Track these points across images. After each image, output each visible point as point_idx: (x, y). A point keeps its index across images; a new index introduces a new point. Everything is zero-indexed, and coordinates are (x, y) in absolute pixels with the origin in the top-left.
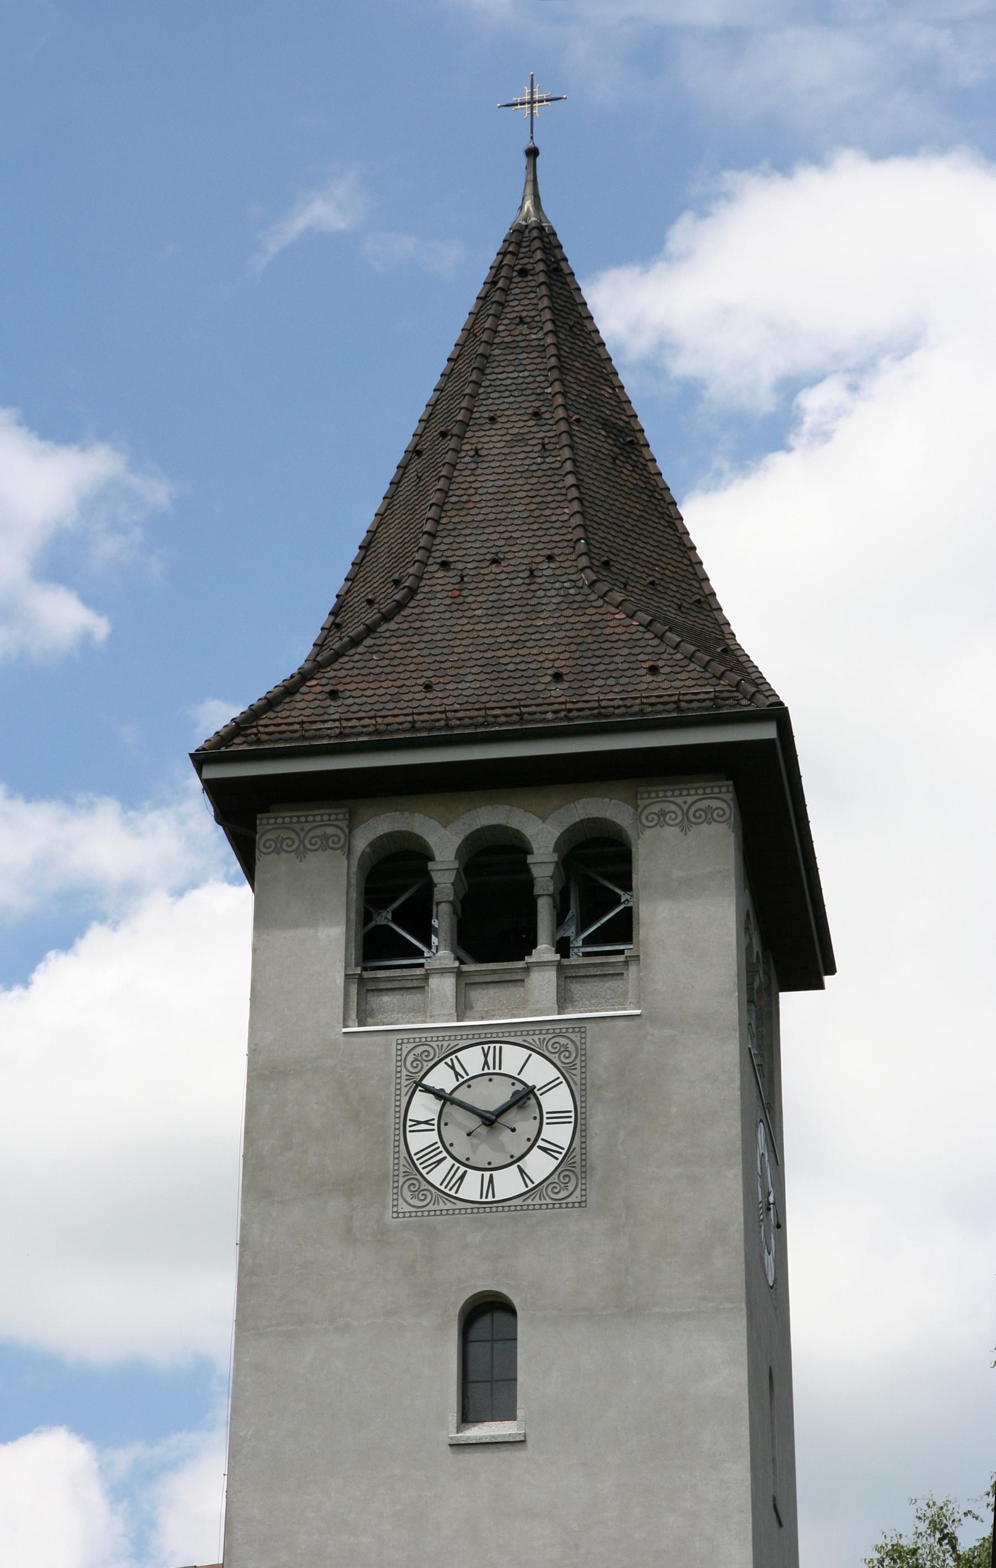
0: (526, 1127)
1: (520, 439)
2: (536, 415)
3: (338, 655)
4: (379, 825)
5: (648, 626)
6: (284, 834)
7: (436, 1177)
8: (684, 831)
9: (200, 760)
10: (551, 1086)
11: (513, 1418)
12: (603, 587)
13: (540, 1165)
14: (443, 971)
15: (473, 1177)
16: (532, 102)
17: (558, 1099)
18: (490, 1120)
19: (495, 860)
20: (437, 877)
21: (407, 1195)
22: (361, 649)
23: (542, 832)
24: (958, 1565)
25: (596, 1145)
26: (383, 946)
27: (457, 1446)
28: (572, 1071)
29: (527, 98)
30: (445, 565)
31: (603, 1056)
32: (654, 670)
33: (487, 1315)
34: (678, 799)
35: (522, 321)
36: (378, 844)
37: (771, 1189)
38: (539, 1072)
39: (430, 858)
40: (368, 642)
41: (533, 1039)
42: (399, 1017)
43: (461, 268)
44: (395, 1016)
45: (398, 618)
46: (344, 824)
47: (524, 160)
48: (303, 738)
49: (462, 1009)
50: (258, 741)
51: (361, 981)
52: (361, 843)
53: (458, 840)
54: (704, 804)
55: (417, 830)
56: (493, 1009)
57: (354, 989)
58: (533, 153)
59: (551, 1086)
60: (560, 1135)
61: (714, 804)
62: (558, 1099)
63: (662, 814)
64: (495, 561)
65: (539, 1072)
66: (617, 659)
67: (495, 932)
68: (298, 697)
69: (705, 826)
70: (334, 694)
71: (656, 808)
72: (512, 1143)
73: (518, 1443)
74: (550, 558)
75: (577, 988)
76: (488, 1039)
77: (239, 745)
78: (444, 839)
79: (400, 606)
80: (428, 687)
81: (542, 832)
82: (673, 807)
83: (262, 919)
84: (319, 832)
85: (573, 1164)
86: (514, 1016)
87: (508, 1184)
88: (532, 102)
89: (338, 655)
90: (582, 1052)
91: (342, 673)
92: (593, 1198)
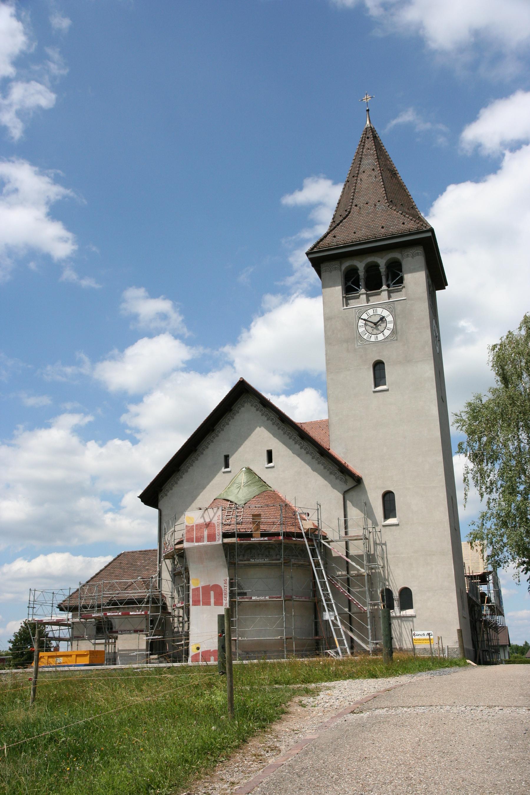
0: (383, 325)
2: (373, 170)
4: (347, 264)
5: (401, 214)
7: (365, 337)
10: (388, 316)
13: (387, 333)
17: (390, 318)
18: (375, 324)
23: (382, 262)
25: (399, 327)
26: (350, 290)
27: (374, 392)
28: (392, 312)
30: (356, 206)
31: (399, 307)
32: (403, 223)
33: (379, 368)
36: (346, 268)
40: (341, 224)
42: (353, 303)
51: (346, 297)
52: (343, 268)
53: (364, 265)
54: (417, 252)
56: (374, 300)
57: (344, 299)
59: (388, 316)
60: (391, 326)
61: (419, 251)
62: (390, 318)
63: (408, 255)
64: (367, 203)
67: (373, 285)
70: (335, 237)
73: (273, 467)
74: (379, 201)
76: (374, 307)
77: (315, 250)
78: (361, 265)
80: (355, 233)
81: (382, 262)
85: (394, 332)
87: (381, 337)
88: (53, 631)
90: (394, 308)
92: (399, 338)
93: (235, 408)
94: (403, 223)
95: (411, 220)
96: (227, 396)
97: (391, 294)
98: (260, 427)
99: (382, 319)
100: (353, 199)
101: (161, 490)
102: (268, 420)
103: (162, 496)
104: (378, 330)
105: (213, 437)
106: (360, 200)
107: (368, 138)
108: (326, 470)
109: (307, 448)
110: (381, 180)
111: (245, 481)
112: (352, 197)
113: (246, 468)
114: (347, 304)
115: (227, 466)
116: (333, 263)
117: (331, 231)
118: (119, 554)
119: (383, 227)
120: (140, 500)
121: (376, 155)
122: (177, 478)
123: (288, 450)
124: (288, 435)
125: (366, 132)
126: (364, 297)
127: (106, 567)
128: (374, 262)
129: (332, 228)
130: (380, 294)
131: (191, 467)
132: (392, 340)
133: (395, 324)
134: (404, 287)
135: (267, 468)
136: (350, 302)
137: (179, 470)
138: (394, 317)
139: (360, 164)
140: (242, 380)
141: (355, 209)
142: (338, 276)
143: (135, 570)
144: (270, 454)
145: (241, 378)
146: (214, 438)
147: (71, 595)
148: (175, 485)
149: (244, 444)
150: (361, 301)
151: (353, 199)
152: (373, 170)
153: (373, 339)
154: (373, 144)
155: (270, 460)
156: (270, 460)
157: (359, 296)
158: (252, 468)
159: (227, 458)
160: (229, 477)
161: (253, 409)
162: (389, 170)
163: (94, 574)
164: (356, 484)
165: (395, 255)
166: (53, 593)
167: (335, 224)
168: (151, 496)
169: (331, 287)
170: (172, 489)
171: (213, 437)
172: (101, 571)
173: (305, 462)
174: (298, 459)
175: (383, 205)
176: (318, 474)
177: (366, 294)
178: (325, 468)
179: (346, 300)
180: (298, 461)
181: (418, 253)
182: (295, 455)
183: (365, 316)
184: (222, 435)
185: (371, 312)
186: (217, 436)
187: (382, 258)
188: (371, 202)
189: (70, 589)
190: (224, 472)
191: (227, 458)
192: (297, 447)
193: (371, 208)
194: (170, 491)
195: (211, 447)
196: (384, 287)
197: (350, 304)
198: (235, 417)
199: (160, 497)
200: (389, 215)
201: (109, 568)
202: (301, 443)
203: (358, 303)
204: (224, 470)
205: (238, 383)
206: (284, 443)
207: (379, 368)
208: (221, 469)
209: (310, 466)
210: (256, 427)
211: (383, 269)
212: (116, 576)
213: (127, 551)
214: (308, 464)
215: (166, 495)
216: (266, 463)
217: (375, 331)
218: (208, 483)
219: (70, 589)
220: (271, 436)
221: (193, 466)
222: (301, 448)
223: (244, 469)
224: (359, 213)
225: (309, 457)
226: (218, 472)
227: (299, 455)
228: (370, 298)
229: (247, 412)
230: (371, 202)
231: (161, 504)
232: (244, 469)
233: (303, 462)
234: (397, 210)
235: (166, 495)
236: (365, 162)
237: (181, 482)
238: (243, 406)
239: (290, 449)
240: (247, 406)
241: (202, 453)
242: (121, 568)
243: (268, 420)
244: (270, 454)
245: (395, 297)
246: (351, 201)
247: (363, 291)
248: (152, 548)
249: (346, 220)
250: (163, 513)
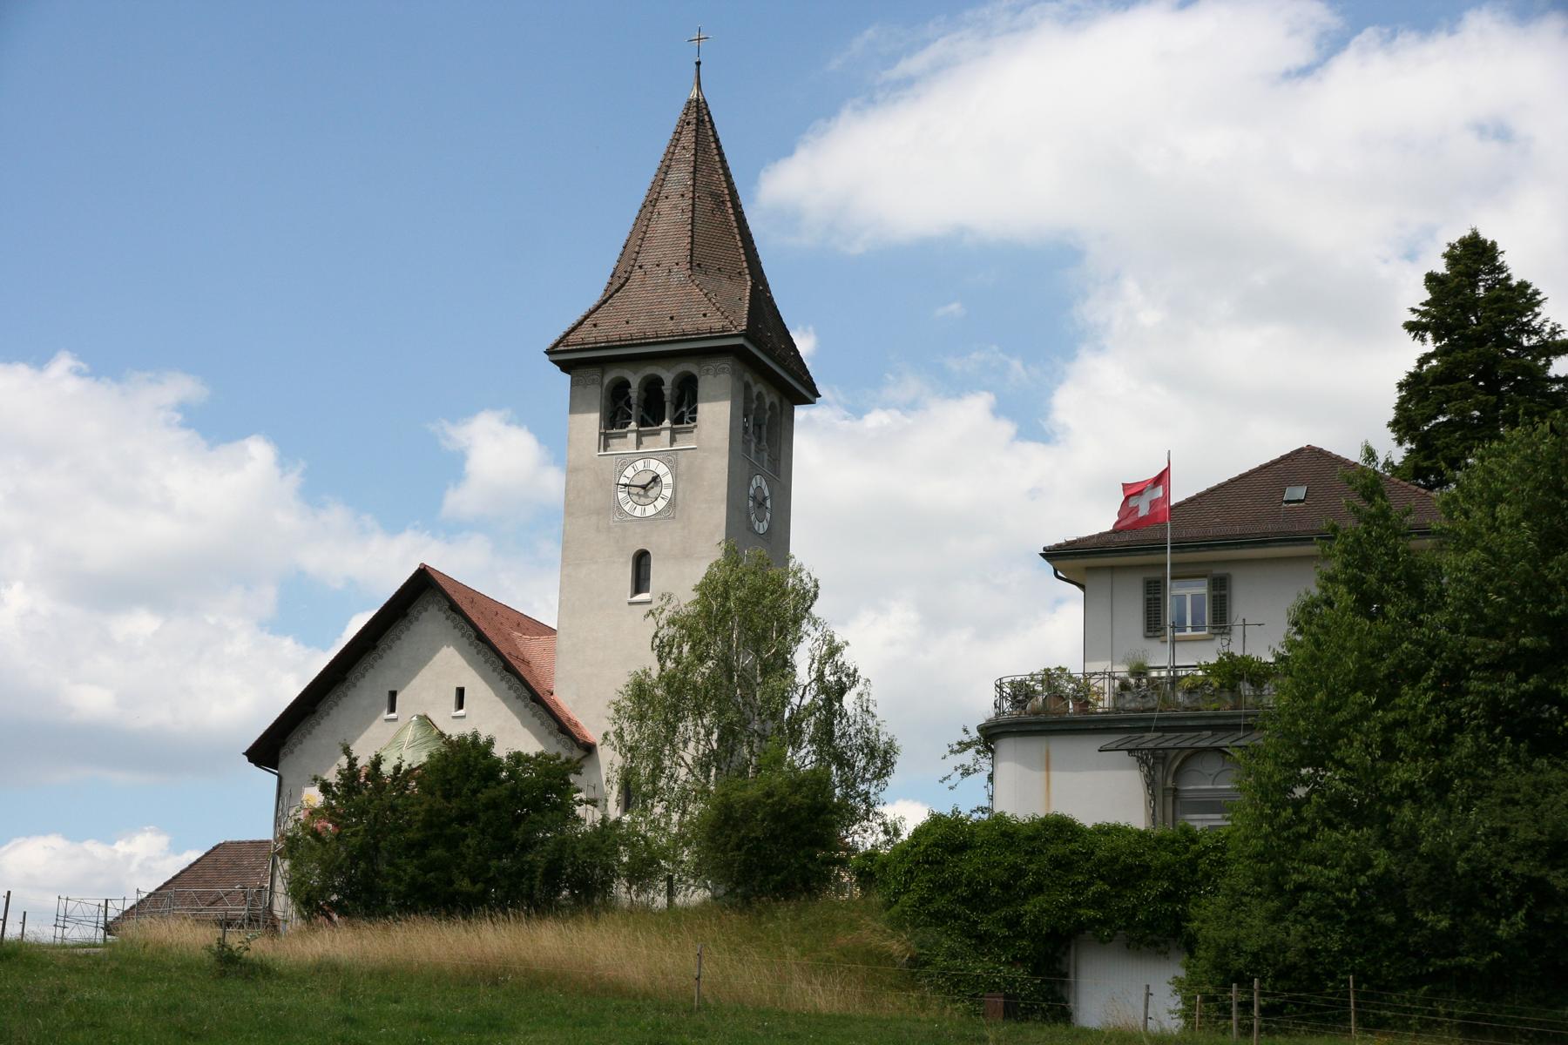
0: (656, 490)
1: (675, 207)
4: (612, 374)
7: (626, 508)
9: (548, 352)
13: (661, 504)
17: (667, 479)
18: (644, 487)
19: (652, 387)
23: (668, 376)
25: (679, 496)
26: (614, 420)
28: (674, 469)
31: (683, 461)
33: (641, 561)
36: (611, 381)
38: (662, 469)
43: (673, 115)
49: (639, 443)
52: (606, 381)
56: (650, 444)
58: (698, 63)
60: (667, 492)
62: (667, 479)
67: (651, 415)
73: (463, 717)
76: (646, 456)
77: (561, 348)
78: (635, 379)
81: (668, 376)
83: (573, 384)
85: (672, 503)
87: (650, 510)
93: (413, 612)
99: (656, 479)
101: (284, 744)
106: (647, 259)
114: (606, 446)
115: (392, 710)
116: (591, 370)
117: (605, 302)
126: (632, 437)
133: (675, 491)
136: (613, 442)
137: (314, 712)
138: (675, 478)
141: (638, 273)
142: (596, 394)
144: (461, 692)
155: (460, 705)
156: (460, 705)
160: (393, 727)
161: (442, 616)
162: (712, 194)
175: (681, 273)
179: (606, 439)
183: (623, 481)
185: (640, 465)
186: (381, 657)
188: (665, 263)
192: (504, 685)
193: (661, 273)
195: (370, 675)
196: (667, 423)
200: (687, 294)
204: (386, 715)
207: (641, 561)
214: (518, 714)
224: (643, 283)
225: (520, 704)
226: (375, 718)
227: (505, 700)
229: (429, 621)
230: (665, 263)
236: (673, 176)
237: (317, 731)
244: (461, 692)
245: (684, 442)
248: (265, 838)
250: (285, 782)
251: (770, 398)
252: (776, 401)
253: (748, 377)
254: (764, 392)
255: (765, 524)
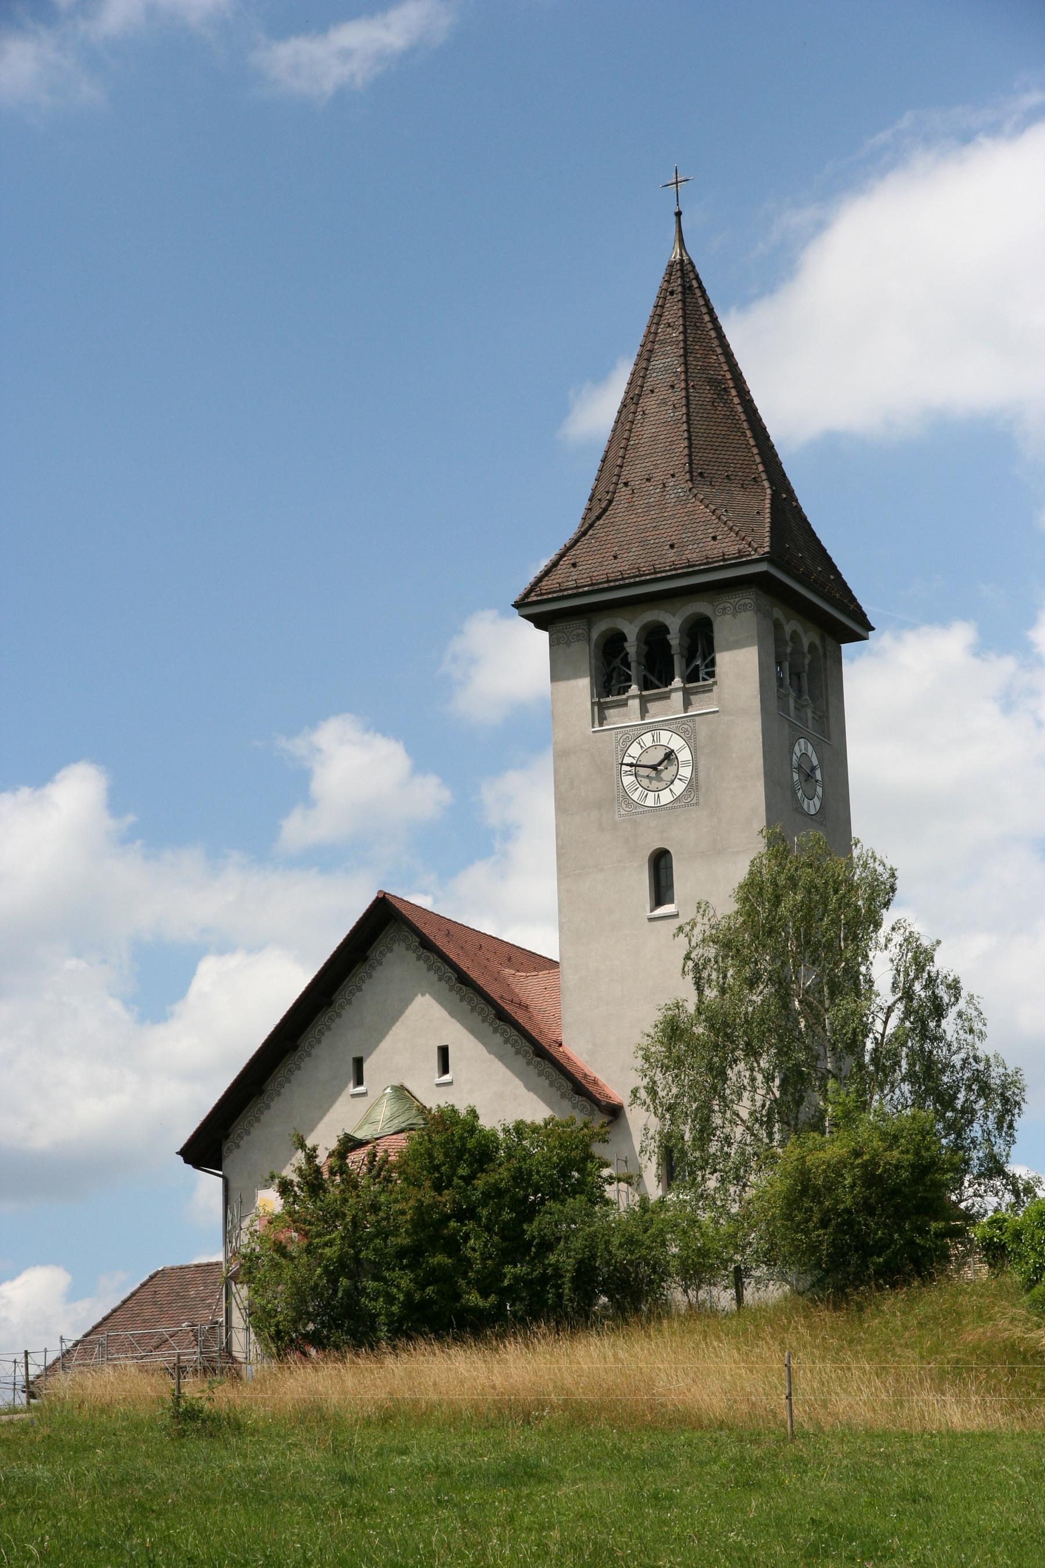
0: (672, 769)
1: (664, 402)
2: (672, 387)
3: (591, 526)
4: (602, 626)
5: (713, 512)
6: (560, 635)
7: (635, 797)
8: (734, 616)
10: (681, 749)
11: (672, 902)
12: (695, 491)
13: (679, 787)
14: (633, 697)
15: (651, 795)
16: (677, 183)
17: (684, 755)
18: (654, 767)
20: (628, 650)
21: (624, 806)
22: (587, 537)
23: (674, 621)
24: (3, 1426)
25: (702, 775)
26: (609, 684)
27: (651, 919)
29: (674, 181)
30: (626, 484)
31: (703, 729)
32: (714, 538)
33: (660, 864)
34: (730, 601)
35: (669, 326)
37: (815, 762)
38: (676, 743)
39: (626, 640)
40: (591, 532)
41: (673, 727)
42: (617, 718)
44: (615, 719)
45: (604, 517)
46: (586, 627)
47: (674, 218)
48: (561, 591)
49: (644, 712)
50: (542, 594)
51: (599, 704)
52: (595, 635)
53: (636, 630)
54: (742, 602)
55: (661, 619)
56: (658, 712)
57: (596, 708)
58: (678, 214)
59: (681, 749)
60: (686, 772)
61: (748, 601)
62: (684, 755)
63: (724, 609)
64: (648, 480)
65: (676, 743)
66: (699, 533)
67: (656, 673)
68: (559, 567)
69: (743, 614)
70: (574, 565)
71: (721, 606)
72: (666, 775)
73: (450, 1083)
74: (673, 476)
75: (693, 698)
76: (654, 728)
78: (631, 629)
79: (605, 510)
80: (615, 557)
81: (674, 621)
82: (729, 605)
84: (575, 632)
85: (693, 785)
86: (667, 715)
87: (666, 797)
88: (677, 183)
89: (591, 526)
90: (694, 731)
91: (578, 552)
92: (701, 800)
93: (374, 954)
94: (714, 538)
95: (731, 529)
96: (326, 964)
97: (692, 697)
98: (423, 995)
100: (621, 467)
102: (440, 980)
103: (228, 1148)
104: (660, 780)
105: (330, 1018)
106: (634, 473)
107: (672, 293)
108: (554, 1089)
109: (516, 1041)
110: (684, 419)
111: (388, 1114)
112: (619, 462)
113: (394, 1088)
114: (602, 720)
115: (359, 1082)
117: (584, 534)
118: (152, 1272)
119: (672, 546)
120: (180, 1158)
121: (682, 345)
122: (259, 1110)
123: (481, 1046)
124: (480, 1014)
125: (671, 274)
127: (124, 1302)
128: (654, 621)
129: (597, 512)
130: (668, 698)
131: (286, 1085)
132: (688, 805)
134: (715, 683)
135: (438, 1085)
136: (610, 713)
139: (646, 369)
140: (381, 896)
141: (624, 492)
143: (184, 1307)
144: (444, 1052)
145: (380, 891)
146: (353, 995)
147: (50, 1367)
148: (256, 1125)
149: (391, 1032)
150: (627, 715)
151: (621, 467)
152: (672, 387)
153: (650, 801)
154: (680, 313)
155: (445, 1069)
156: (445, 1069)
157: (627, 699)
158: (408, 1085)
159: (358, 1063)
160: (363, 1104)
161: (411, 956)
163: (100, 1319)
164: (611, 1118)
165: (700, 607)
166: (15, 1362)
167: (599, 509)
168: (206, 1148)
169: (568, 678)
170: (248, 1133)
171: (330, 1018)
172: (114, 1311)
173: (513, 1072)
174: (499, 1065)
175: (679, 486)
176: (539, 1097)
177: (641, 697)
178: (551, 1085)
179: (600, 711)
180: (499, 1070)
181: (745, 604)
182: (492, 1056)
183: (627, 760)
184: (349, 1014)
185: (647, 739)
187: (674, 615)
188: (658, 476)
189: (46, 1351)
190: (353, 1096)
191: (359, 1063)
194: (246, 1138)
197: (609, 720)
198: (374, 974)
199: (225, 1149)
200: (689, 514)
201: (129, 1305)
202: (505, 1031)
203: (625, 715)
204: (351, 1089)
205: (374, 902)
206: (472, 1031)
207: (660, 864)
208: (346, 1086)
209: (521, 1080)
210: (416, 995)
211: (674, 639)
212: (144, 1321)
213: (169, 1266)
215: (238, 1146)
216: (437, 1075)
217: (655, 784)
218: (321, 1118)
219: (46, 1351)
220: (445, 1014)
221: (289, 1082)
222: (506, 1042)
223: (388, 1090)
225: (521, 1061)
227: (501, 1058)
228: (649, 705)
229: (397, 964)
230: (658, 476)
231: (226, 1163)
232: (388, 1090)
233: (509, 1073)
234: (707, 502)
235: (238, 1146)
236: (657, 363)
238: (391, 950)
239: (484, 1044)
240: (399, 948)
241: (309, 1055)
242: (155, 1303)
243: (440, 980)
244: (444, 1052)
245: (702, 705)
246: (616, 471)
247: (634, 689)
249: (601, 522)
250: (233, 1185)
251: (809, 637)
252: (817, 642)
253: (778, 613)
254: (800, 630)
255: (817, 802)
